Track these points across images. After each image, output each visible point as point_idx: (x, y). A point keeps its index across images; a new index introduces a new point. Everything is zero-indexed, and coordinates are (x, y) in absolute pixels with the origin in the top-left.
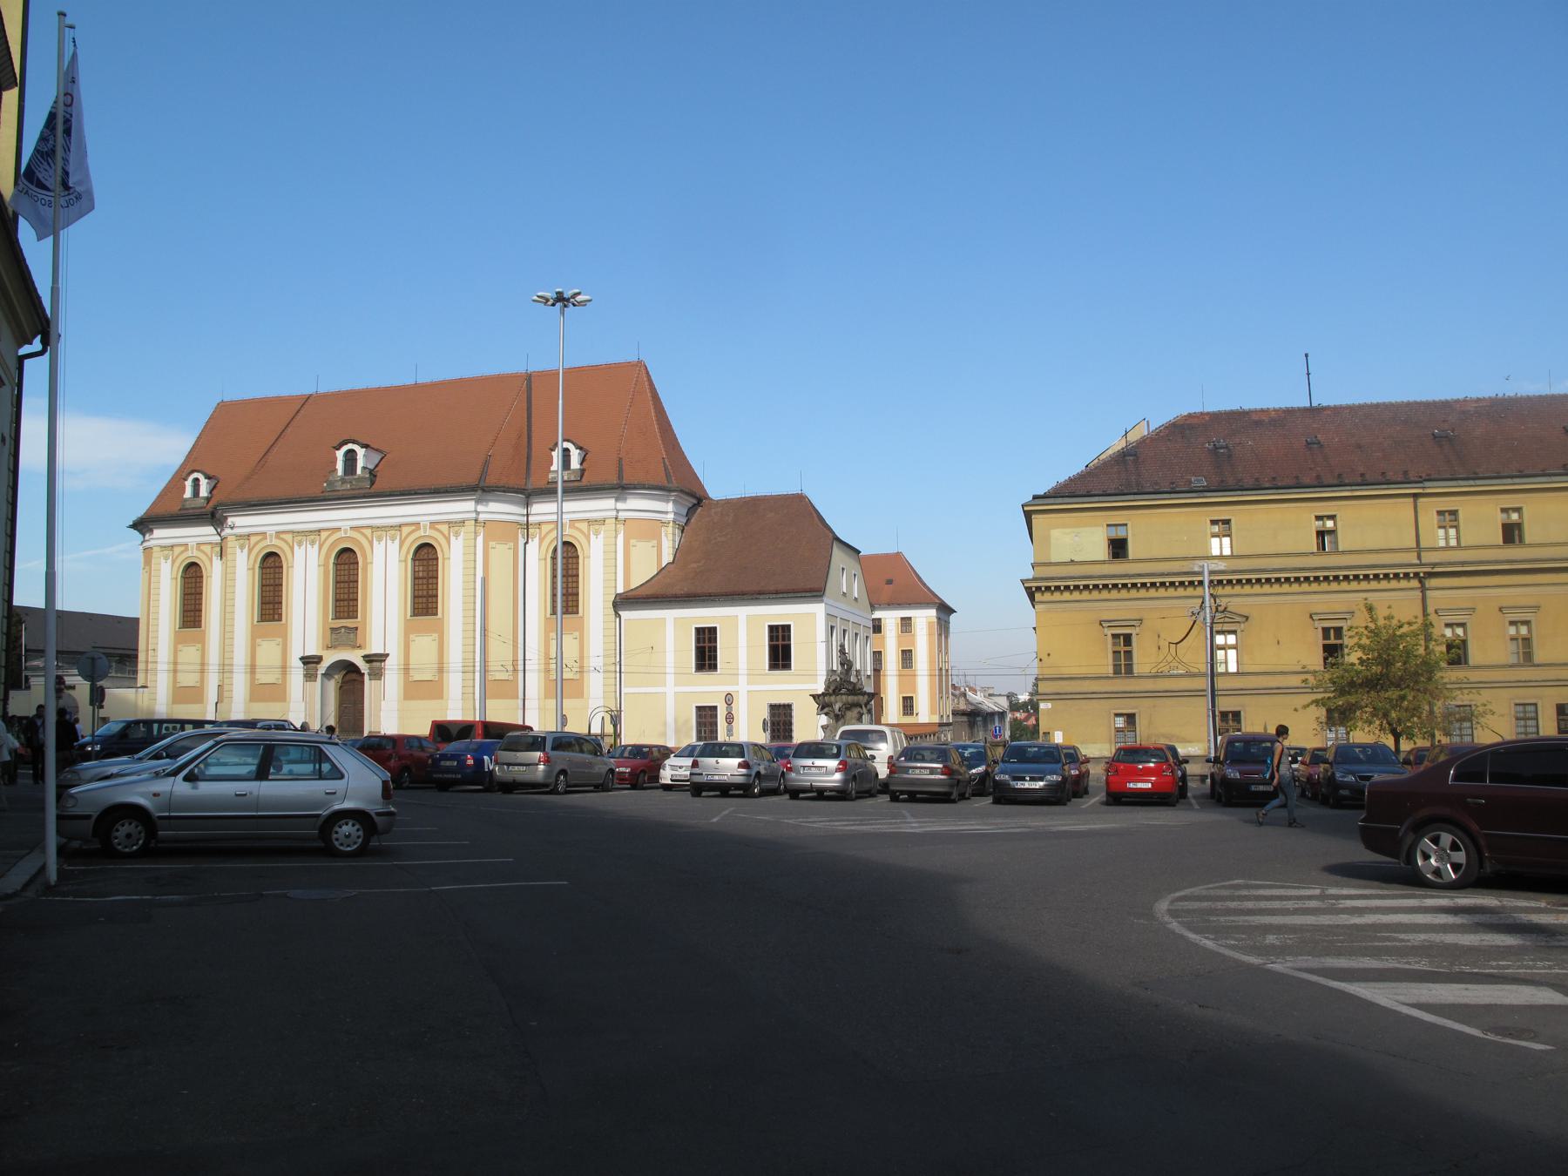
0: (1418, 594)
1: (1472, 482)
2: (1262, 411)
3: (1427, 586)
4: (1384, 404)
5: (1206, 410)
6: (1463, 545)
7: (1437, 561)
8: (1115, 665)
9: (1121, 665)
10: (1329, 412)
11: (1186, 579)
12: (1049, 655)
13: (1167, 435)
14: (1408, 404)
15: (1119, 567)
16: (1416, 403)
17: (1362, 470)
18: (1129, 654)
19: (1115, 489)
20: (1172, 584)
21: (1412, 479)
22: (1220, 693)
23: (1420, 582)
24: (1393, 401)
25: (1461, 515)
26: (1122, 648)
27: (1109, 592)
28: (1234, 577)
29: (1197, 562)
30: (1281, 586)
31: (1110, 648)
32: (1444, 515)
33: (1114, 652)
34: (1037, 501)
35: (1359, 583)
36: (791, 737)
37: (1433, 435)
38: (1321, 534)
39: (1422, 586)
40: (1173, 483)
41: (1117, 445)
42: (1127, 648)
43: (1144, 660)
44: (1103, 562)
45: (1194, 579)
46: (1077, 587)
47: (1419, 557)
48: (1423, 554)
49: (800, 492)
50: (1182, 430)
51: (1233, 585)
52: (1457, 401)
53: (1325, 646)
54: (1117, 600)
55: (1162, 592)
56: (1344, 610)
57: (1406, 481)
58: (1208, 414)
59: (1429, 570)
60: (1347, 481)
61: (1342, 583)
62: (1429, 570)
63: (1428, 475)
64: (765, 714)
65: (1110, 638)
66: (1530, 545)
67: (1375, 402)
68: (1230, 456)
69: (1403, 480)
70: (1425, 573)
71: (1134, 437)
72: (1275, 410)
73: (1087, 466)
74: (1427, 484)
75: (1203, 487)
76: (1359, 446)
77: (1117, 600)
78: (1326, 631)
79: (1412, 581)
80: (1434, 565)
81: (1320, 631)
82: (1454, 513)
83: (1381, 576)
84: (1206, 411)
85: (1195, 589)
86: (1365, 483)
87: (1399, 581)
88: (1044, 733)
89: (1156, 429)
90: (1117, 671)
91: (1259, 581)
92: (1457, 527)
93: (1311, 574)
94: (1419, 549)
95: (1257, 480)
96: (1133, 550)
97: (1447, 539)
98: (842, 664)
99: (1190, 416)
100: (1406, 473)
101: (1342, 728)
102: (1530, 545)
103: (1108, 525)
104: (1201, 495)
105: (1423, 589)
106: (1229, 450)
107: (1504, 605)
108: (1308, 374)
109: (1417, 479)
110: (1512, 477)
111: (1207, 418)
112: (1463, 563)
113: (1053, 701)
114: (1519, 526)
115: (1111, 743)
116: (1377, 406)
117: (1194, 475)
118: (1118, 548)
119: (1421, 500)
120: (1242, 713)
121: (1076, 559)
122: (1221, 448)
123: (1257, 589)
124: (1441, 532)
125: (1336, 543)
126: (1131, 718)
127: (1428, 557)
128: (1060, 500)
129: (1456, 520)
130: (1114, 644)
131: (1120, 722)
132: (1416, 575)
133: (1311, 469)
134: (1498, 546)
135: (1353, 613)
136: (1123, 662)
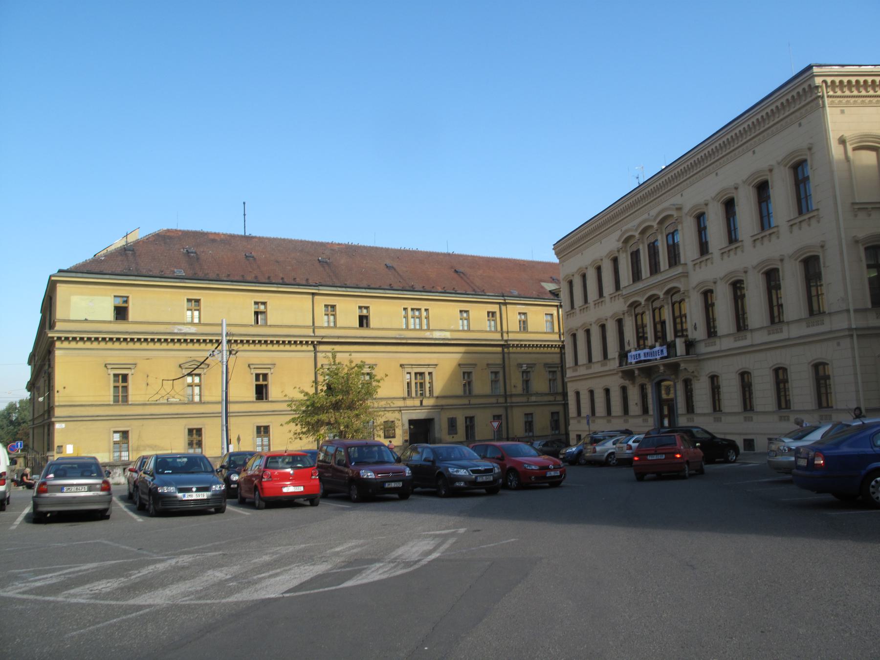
0: (313, 354)
1: (344, 289)
2: (215, 233)
3: (318, 350)
4: (288, 239)
5: (179, 229)
6: (202, 322)
7: (324, 335)
8: (114, 396)
9: (119, 396)
10: (256, 240)
11: (169, 337)
12: (64, 388)
13: (154, 240)
14: (301, 241)
15: (121, 326)
16: (305, 241)
17: (281, 275)
18: (125, 388)
19: (121, 271)
20: (159, 340)
21: (311, 284)
22: (231, 414)
23: (314, 347)
24: (293, 239)
25: (338, 308)
26: (120, 384)
27: (113, 343)
28: (202, 338)
29: (176, 326)
30: (181, 344)
31: (112, 384)
32: (327, 308)
33: (115, 387)
34: (62, 274)
35: (279, 346)
37: (318, 260)
38: (257, 313)
39: (315, 350)
40: (162, 272)
41: (119, 243)
42: (125, 384)
43: (136, 393)
44: (110, 322)
45: (231, 338)
46: (89, 339)
47: (314, 332)
48: (316, 330)
50: (164, 238)
51: (77, 341)
52: (328, 243)
53: (257, 385)
54: (97, 349)
55: (151, 345)
56: (270, 363)
57: (308, 285)
58: (180, 231)
60: (274, 281)
61: (303, 346)
62: (319, 340)
63: (320, 283)
64: (454, 416)
65: (112, 377)
66: (373, 329)
67: (283, 237)
68: (198, 259)
69: (306, 284)
70: (317, 342)
71: (132, 239)
72: (224, 235)
73: (95, 255)
74: (321, 288)
75: (183, 276)
76: (277, 262)
77: (97, 349)
78: (257, 376)
79: (309, 346)
80: (323, 337)
81: (254, 375)
82: (198, 301)
83: (202, 341)
84: (179, 229)
85: (106, 344)
86: (284, 284)
87: (302, 346)
88: (58, 446)
89: (146, 236)
90: (116, 401)
91: (111, 339)
92: (199, 310)
93: (128, 337)
94: (314, 327)
95: (218, 275)
96: (132, 315)
97: (192, 317)
99: (168, 231)
100: (307, 280)
101: (266, 438)
102: (373, 329)
103: (115, 296)
104: (182, 281)
105: (315, 351)
106: (197, 254)
107: (251, 363)
108: (245, 215)
109: (314, 284)
110: (365, 288)
111: (180, 234)
112: (339, 337)
113: (66, 422)
114: (367, 317)
115: (110, 452)
116: (284, 240)
117: (176, 267)
118: (121, 313)
119: (316, 297)
120: (203, 430)
121: (90, 318)
122: (192, 253)
123: (158, 346)
124: (189, 313)
125: (266, 320)
126: (125, 434)
127: (319, 332)
128: (80, 275)
129: (334, 311)
130: (115, 381)
131: (117, 437)
132: (312, 342)
133: (250, 272)
134: (356, 328)
135: (275, 364)
136: (121, 394)
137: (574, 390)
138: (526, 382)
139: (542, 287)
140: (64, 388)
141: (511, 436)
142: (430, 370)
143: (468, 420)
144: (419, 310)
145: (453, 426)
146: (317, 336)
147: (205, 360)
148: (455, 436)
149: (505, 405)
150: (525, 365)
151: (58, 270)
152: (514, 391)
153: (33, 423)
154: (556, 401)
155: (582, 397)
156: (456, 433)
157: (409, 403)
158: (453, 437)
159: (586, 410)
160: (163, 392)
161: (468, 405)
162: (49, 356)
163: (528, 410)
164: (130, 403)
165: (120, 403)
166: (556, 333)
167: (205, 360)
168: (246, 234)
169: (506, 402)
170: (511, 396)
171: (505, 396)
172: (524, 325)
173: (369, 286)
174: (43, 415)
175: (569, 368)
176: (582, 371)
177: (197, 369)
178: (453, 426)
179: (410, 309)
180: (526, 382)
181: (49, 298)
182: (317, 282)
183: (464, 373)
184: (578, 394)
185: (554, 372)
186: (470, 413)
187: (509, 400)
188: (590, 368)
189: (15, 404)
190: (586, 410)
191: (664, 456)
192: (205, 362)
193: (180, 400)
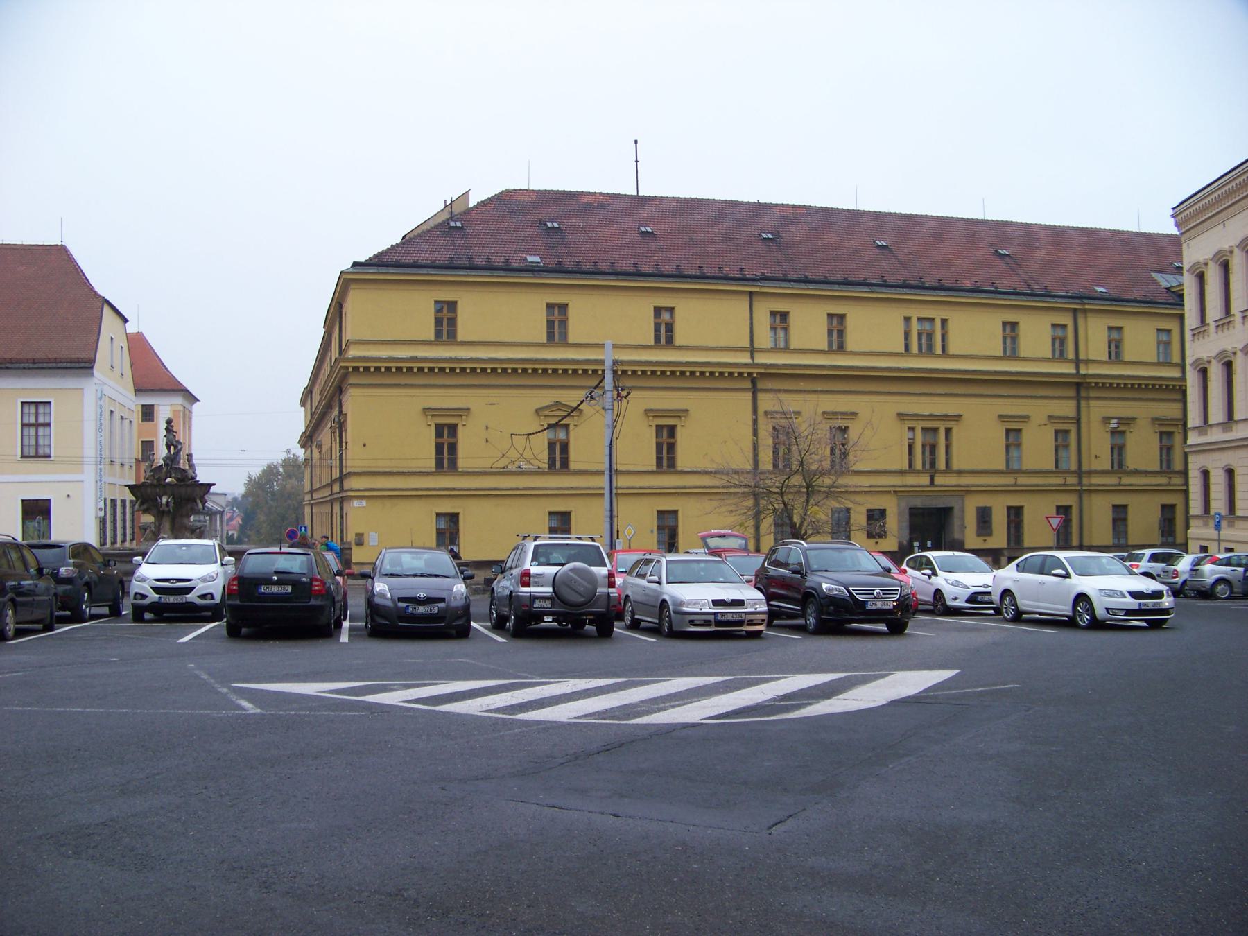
18: (671, 447)
26: (446, 439)
36: (50, 539)
49: (60, 243)
58: (533, 191)
59: (763, 371)
70: (758, 373)
73: (404, 237)
81: (433, 428)
84: (531, 188)
90: (439, 463)
98: (168, 446)
102: (681, 348)
108: (637, 161)
132: (750, 374)
137: (1223, 465)
138: (1118, 451)
139: (1154, 281)
140: (364, 445)
141: (1086, 543)
142: (949, 425)
143: (1012, 512)
144: (932, 320)
145: (985, 522)
146: (757, 364)
147: (579, 405)
148: (880, 541)
149: (1079, 488)
150: (1115, 421)
151: (351, 263)
152: (1096, 466)
153: (312, 496)
154: (1067, 485)
155: (1212, 480)
156: (990, 534)
157: (911, 480)
158: (877, 543)
159: (1218, 504)
160: (513, 454)
161: (1012, 486)
162: (340, 396)
163: (1119, 500)
164: (460, 470)
165: (445, 470)
166: (1176, 365)
167: (579, 405)
168: (639, 194)
169: (1080, 483)
170: (1090, 473)
171: (1079, 473)
172: (1115, 351)
173: (846, 279)
174: (331, 485)
175: (1194, 428)
176: (1216, 435)
177: (568, 418)
178: (985, 522)
179: (916, 319)
180: (1118, 451)
181: (338, 305)
182: (758, 274)
183: (1057, 432)
184: (1206, 474)
185: (1170, 434)
186: (1015, 501)
187: (1085, 481)
188: (1231, 430)
189: (276, 467)
190: (1218, 504)
191: (289, 589)
192: (579, 408)
193: (539, 468)
